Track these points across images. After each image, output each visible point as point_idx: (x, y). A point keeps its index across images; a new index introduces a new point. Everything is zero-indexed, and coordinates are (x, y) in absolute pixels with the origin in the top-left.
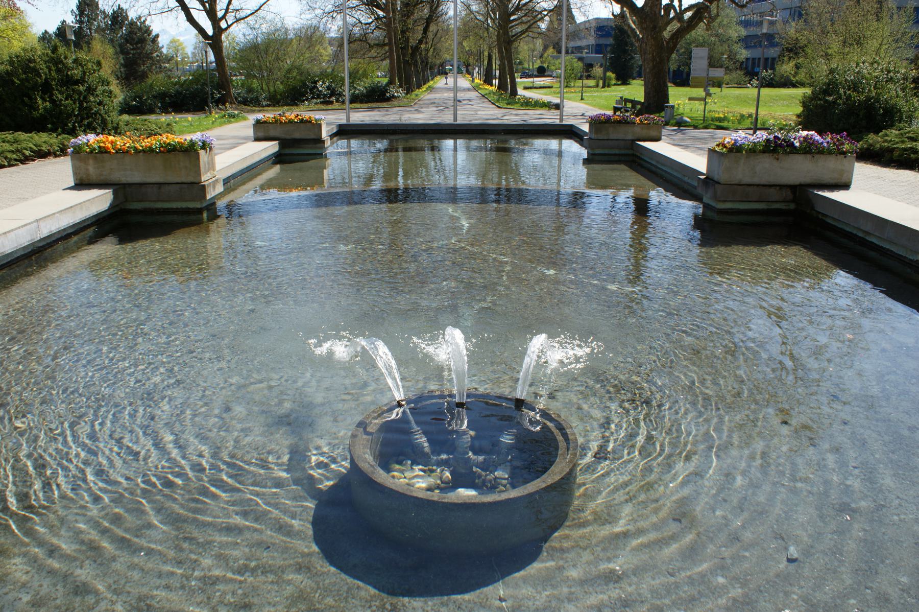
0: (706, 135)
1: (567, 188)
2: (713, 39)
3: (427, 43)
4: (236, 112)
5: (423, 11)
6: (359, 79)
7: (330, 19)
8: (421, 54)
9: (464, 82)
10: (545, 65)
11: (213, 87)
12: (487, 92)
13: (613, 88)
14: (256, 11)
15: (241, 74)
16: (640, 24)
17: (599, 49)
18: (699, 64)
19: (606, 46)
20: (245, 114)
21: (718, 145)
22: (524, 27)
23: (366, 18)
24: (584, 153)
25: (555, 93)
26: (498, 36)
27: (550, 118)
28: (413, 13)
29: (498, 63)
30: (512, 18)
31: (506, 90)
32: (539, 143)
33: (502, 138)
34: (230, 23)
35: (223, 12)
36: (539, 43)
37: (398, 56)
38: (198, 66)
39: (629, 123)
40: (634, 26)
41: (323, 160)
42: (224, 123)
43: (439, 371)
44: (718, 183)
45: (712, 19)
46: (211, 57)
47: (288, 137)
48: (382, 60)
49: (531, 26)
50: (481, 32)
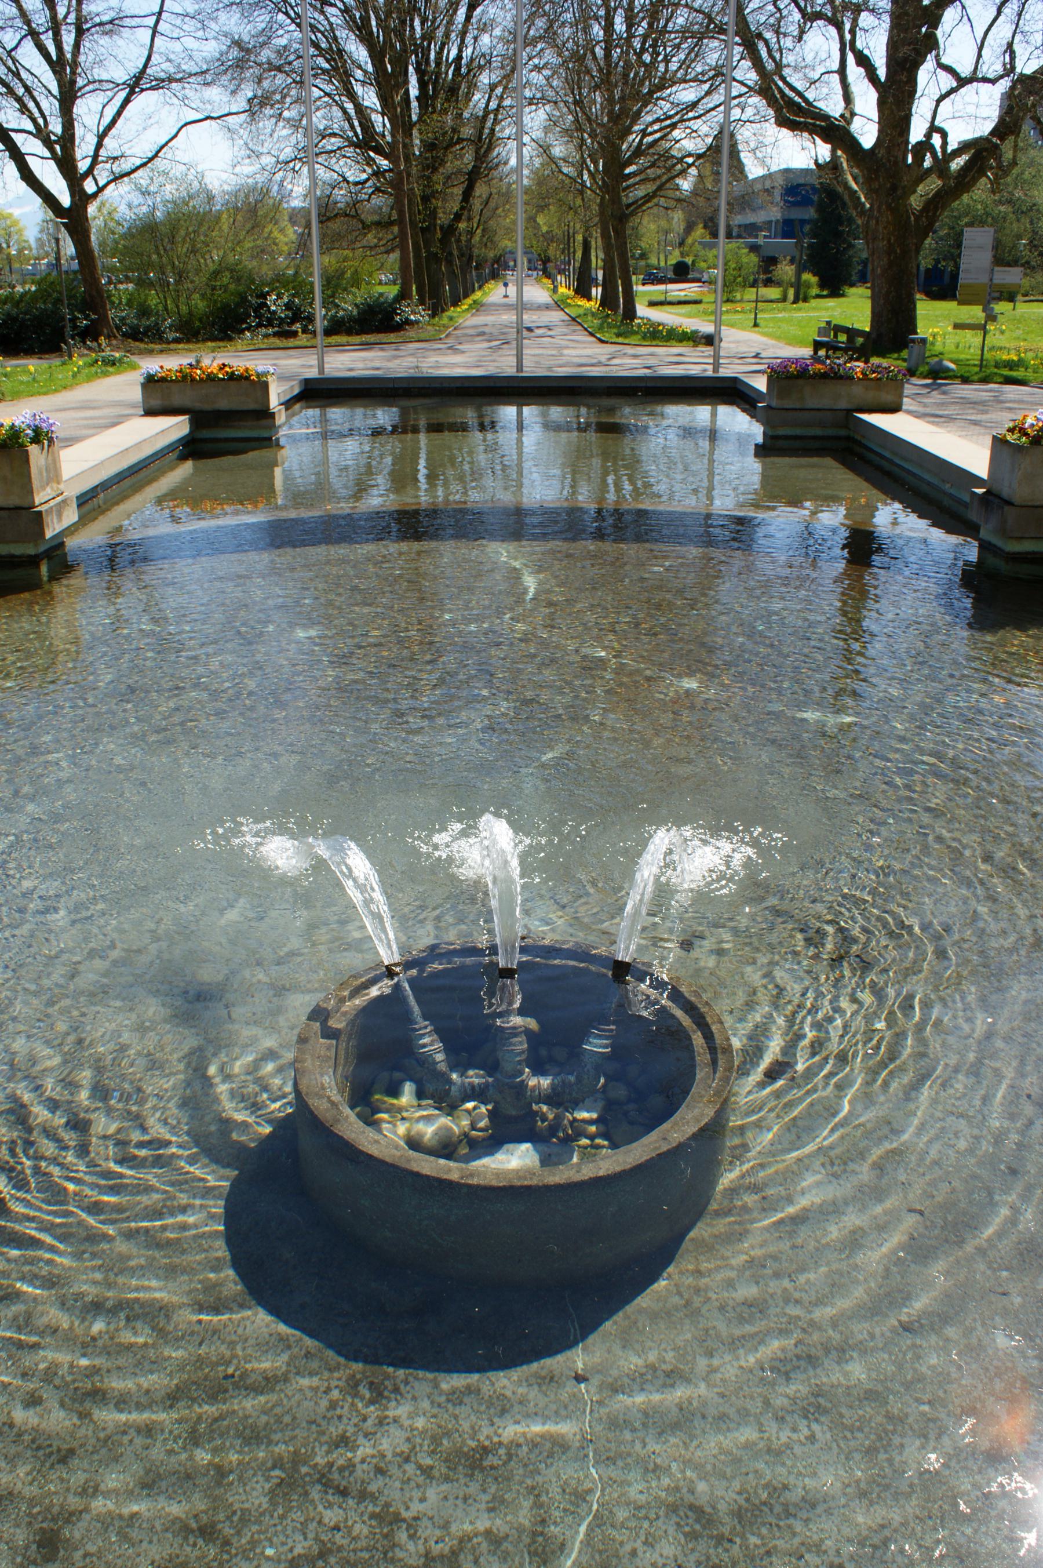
0: (985, 396)
1: (724, 503)
2: (1002, 208)
3: (469, 219)
4: (117, 355)
5: (462, 157)
6: (345, 289)
7: (290, 175)
8: (458, 241)
9: (537, 292)
10: (689, 260)
11: (72, 307)
12: (581, 311)
13: (814, 303)
14: (151, 160)
15: (128, 279)
16: (868, 183)
17: (788, 228)
18: (976, 259)
19: (803, 222)
20: (134, 358)
21: (1011, 430)
22: (650, 187)
23: (354, 174)
24: (756, 431)
25: (705, 313)
26: (601, 205)
27: (694, 363)
28: (443, 163)
29: (601, 255)
30: (627, 171)
31: (614, 308)
32: (677, 413)
33: (604, 404)
34: (101, 184)
35: (89, 160)
36: (678, 217)
37: (416, 245)
38: (48, 265)
39: (841, 377)
40: (855, 187)
41: (275, 449)
42: (96, 376)
43: (471, 896)
44: (1009, 503)
45: (1003, 171)
46: (69, 248)
47: (207, 407)
48: (387, 252)
49: (664, 185)
50: (570, 197)
